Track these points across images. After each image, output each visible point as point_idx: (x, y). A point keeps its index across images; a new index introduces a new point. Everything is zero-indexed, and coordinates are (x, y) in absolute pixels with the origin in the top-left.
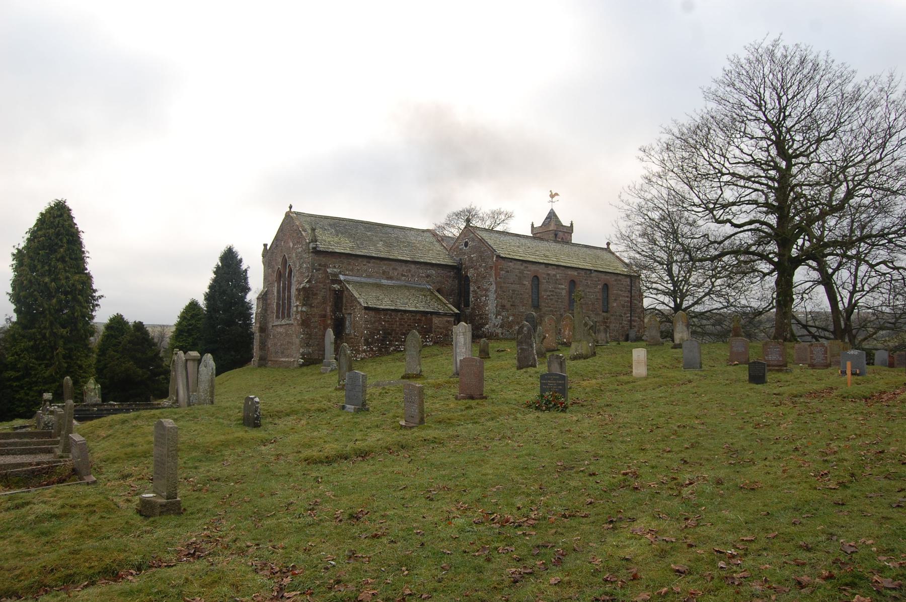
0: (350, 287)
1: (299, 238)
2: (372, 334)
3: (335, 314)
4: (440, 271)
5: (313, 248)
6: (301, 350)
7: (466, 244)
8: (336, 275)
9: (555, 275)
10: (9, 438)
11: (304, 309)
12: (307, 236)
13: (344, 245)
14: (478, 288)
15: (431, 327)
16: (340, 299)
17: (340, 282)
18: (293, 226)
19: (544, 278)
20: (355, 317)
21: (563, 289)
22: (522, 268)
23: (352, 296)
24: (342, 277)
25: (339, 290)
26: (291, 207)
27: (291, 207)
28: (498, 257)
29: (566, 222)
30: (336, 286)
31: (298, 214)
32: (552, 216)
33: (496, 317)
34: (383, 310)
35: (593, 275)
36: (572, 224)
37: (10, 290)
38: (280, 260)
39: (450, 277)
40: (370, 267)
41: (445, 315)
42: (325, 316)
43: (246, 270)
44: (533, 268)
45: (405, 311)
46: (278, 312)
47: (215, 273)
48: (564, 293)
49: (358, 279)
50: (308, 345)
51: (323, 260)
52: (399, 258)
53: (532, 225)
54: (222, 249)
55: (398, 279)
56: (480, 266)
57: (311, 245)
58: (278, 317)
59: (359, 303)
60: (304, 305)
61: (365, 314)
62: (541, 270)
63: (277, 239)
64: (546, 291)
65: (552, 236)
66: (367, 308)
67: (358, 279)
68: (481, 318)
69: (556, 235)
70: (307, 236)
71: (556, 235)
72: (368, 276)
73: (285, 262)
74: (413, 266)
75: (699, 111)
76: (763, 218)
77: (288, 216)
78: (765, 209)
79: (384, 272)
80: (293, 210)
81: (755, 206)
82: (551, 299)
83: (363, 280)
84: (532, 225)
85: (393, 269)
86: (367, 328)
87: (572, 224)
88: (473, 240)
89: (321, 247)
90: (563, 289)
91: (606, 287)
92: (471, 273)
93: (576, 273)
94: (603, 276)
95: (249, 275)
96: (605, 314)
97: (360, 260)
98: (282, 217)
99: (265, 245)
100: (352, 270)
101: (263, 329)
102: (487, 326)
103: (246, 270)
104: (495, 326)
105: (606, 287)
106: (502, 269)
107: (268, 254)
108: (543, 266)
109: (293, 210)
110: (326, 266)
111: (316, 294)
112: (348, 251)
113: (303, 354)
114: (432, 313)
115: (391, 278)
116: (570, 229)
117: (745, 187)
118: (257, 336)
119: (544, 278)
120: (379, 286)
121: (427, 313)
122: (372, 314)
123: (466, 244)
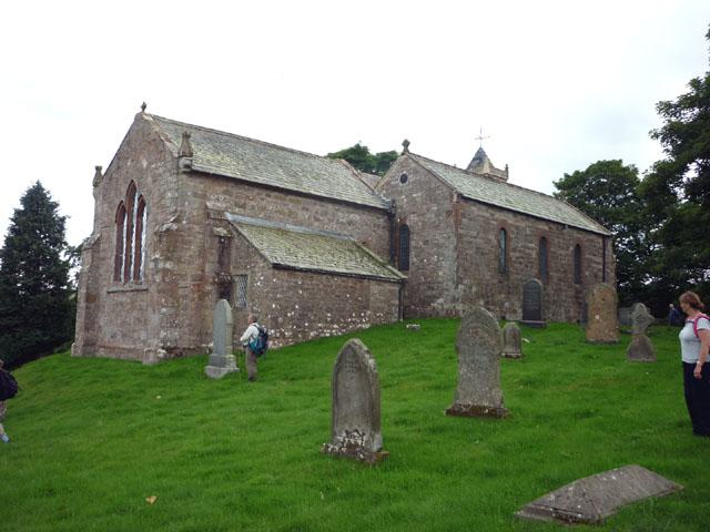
0: (245, 232)
1: (152, 160)
2: (283, 310)
3: (218, 274)
6: (163, 334)
7: (404, 179)
8: (220, 212)
9: (524, 229)
10: (132, 233)
12: (175, 146)
14: (426, 242)
15: (368, 300)
16: (226, 245)
18: (145, 135)
19: (513, 233)
20: (253, 281)
23: (251, 245)
24: (229, 217)
26: (144, 107)
27: (144, 107)
28: (460, 196)
30: (222, 231)
31: (156, 118)
33: (456, 287)
34: (301, 270)
35: (565, 231)
38: (124, 189)
40: (271, 203)
43: (63, 220)
44: (499, 215)
45: (333, 274)
46: (117, 271)
48: (534, 254)
49: (253, 221)
50: (173, 326)
52: (312, 192)
54: (31, 184)
55: (310, 225)
57: (184, 161)
58: (117, 278)
59: (262, 256)
60: (168, 259)
64: (514, 250)
66: (277, 267)
67: (253, 221)
70: (175, 146)
72: (268, 218)
73: (132, 189)
77: (139, 118)
79: (291, 213)
82: (521, 263)
83: (260, 222)
85: (303, 209)
86: (275, 300)
89: (197, 166)
91: (578, 248)
92: (412, 220)
94: (576, 234)
95: (66, 226)
96: (578, 286)
97: (256, 191)
99: (98, 169)
100: (243, 206)
101: (90, 298)
102: (441, 300)
103: (63, 220)
104: (454, 300)
106: (464, 215)
107: (102, 181)
109: (146, 111)
114: (370, 278)
118: (82, 304)
120: (284, 232)
122: (284, 275)
123: (404, 179)
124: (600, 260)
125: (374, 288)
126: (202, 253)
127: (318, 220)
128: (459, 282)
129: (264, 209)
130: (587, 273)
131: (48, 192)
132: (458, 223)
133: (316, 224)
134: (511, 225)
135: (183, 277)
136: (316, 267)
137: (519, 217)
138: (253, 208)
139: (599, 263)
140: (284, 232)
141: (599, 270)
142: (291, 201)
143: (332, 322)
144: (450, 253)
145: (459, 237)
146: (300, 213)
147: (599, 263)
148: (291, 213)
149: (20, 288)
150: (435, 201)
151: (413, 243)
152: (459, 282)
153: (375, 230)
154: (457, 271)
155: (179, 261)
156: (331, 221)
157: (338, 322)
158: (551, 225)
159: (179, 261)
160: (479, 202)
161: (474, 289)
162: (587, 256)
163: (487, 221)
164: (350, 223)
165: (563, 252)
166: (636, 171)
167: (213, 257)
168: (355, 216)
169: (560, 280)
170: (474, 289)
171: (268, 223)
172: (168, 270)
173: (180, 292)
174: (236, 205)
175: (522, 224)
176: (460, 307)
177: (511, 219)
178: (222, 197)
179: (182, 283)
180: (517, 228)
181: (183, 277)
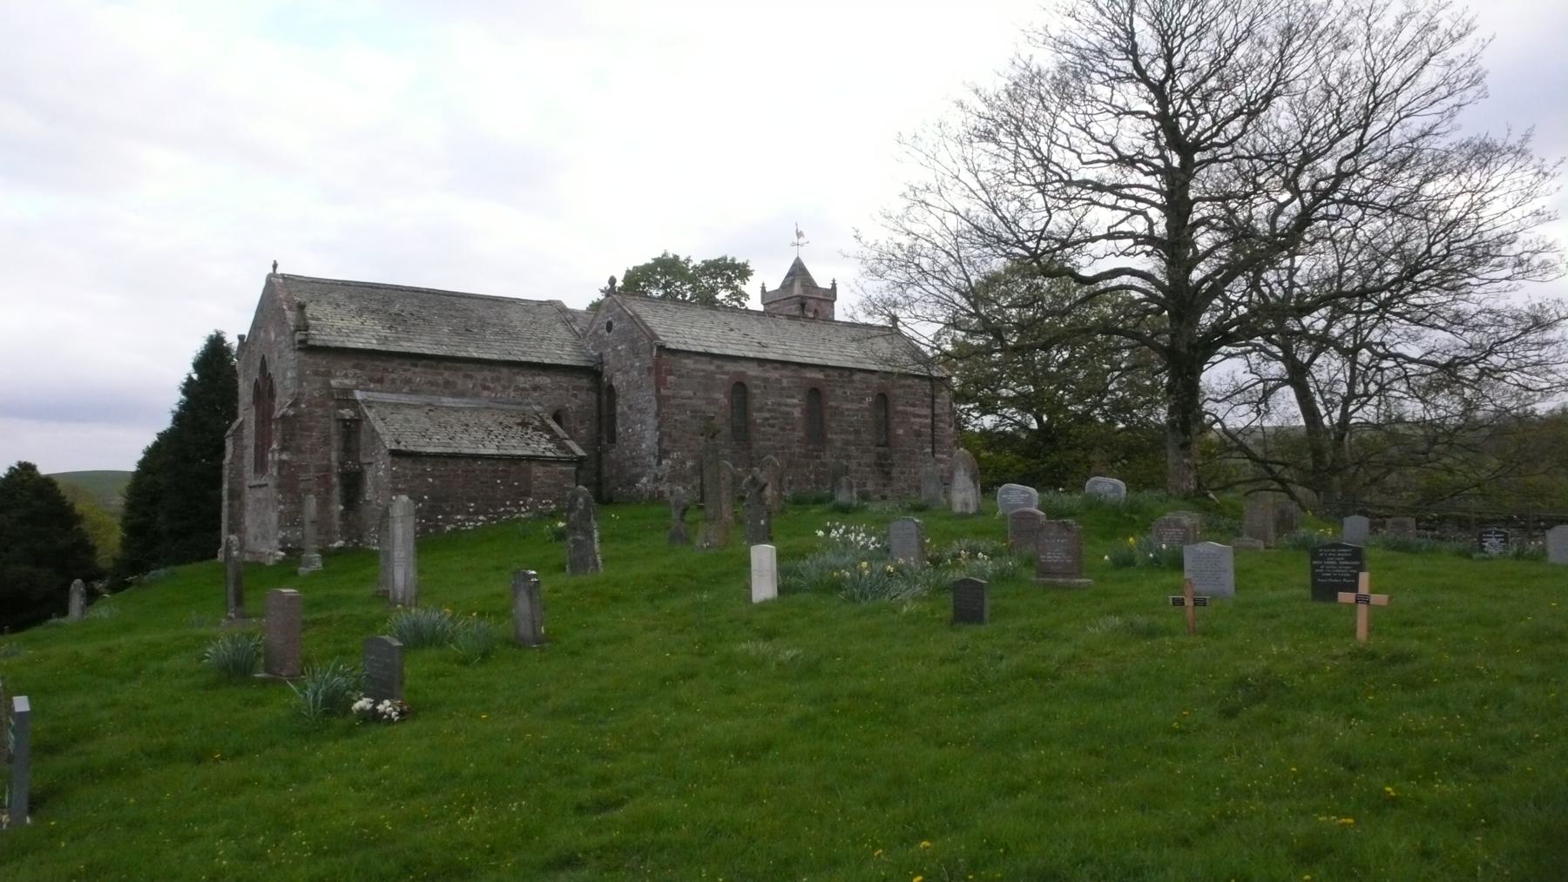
0: (371, 414)
4: (563, 380)
5: (301, 342)
6: (281, 534)
7: (609, 327)
8: (347, 391)
9: (779, 381)
11: (284, 457)
13: (367, 334)
14: (630, 407)
17: (354, 404)
19: (756, 387)
21: (795, 406)
22: (712, 368)
24: (359, 395)
25: (351, 420)
26: (275, 266)
27: (275, 266)
28: (662, 349)
29: (823, 282)
30: (347, 413)
32: (798, 272)
33: (659, 463)
34: (429, 455)
36: (834, 285)
37: (176, 408)
39: (580, 389)
41: (558, 461)
42: (328, 469)
44: (730, 367)
47: (185, 392)
48: (797, 413)
51: (322, 362)
53: (763, 288)
55: (477, 395)
56: (632, 366)
57: (298, 336)
61: (393, 463)
62: (753, 371)
63: (255, 326)
64: (760, 410)
65: (794, 309)
66: (395, 453)
68: (636, 465)
69: (803, 306)
71: (803, 306)
72: (413, 392)
74: (505, 371)
75: (1548, 232)
76: (1124, 262)
78: (1149, 248)
80: (279, 271)
81: (1131, 241)
82: (773, 426)
83: (404, 399)
84: (763, 288)
87: (834, 285)
88: (620, 319)
89: (319, 338)
90: (795, 406)
91: (883, 399)
92: (618, 380)
93: (820, 376)
97: (395, 363)
98: (263, 284)
100: (381, 381)
102: (644, 480)
104: (657, 479)
105: (883, 399)
106: (670, 373)
108: (755, 364)
109: (279, 271)
110: (329, 374)
111: (310, 429)
112: (374, 345)
113: (283, 541)
114: (530, 459)
115: (462, 394)
116: (830, 295)
117: (1114, 207)
119: (756, 387)
121: (520, 458)
122: (407, 463)
123: (609, 327)
124: (927, 411)
125: (538, 471)
126: (326, 440)
127: (488, 388)
128: (663, 454)
129: (408, 381)
130: (901, 432)
131: (688, 260)
132: (660, 382)
133: (486, 393)
134: (756, 378)
135: (305, 469)
136: (450, 450)
137: (768, 366)
138: (393, 381)
139: (925, 417)
140: (433, 408)
141: (924, 426)
142: (446, 369)
143: (477, 513)
144: (651, 421)
145: (662, 400)
146: (460, 382)
147: (925, 417)
148: (447, 383)
149: (1040, 421)
150: (637, 355)
151: (619, 409)
152: (663, 454)
153: (577, 399)
154: (660, 442)
155: (299, 451)
156: (505, 388)
157: (485, 513)
158: (830, 372)
159: (299, 451)
160: (689, 352)
161: (689, 464)
162: (900, 408)
163: (710, 376)
164: (536, 388)
165: (855, 406)
166: (1044, 261)
167: (336, 442)
168: (545, 380)
169: (847, 443)
170: (689, 464)
171: (414, 400)
172: (284, 462)
173: (302, 485)
174: (371, 380)
175: (774, 375)
176: (665, 488)
177: (753, 371)
178: (351, 372)
179: (303, 476)
180: (766, 380)
181: (305, 469)
